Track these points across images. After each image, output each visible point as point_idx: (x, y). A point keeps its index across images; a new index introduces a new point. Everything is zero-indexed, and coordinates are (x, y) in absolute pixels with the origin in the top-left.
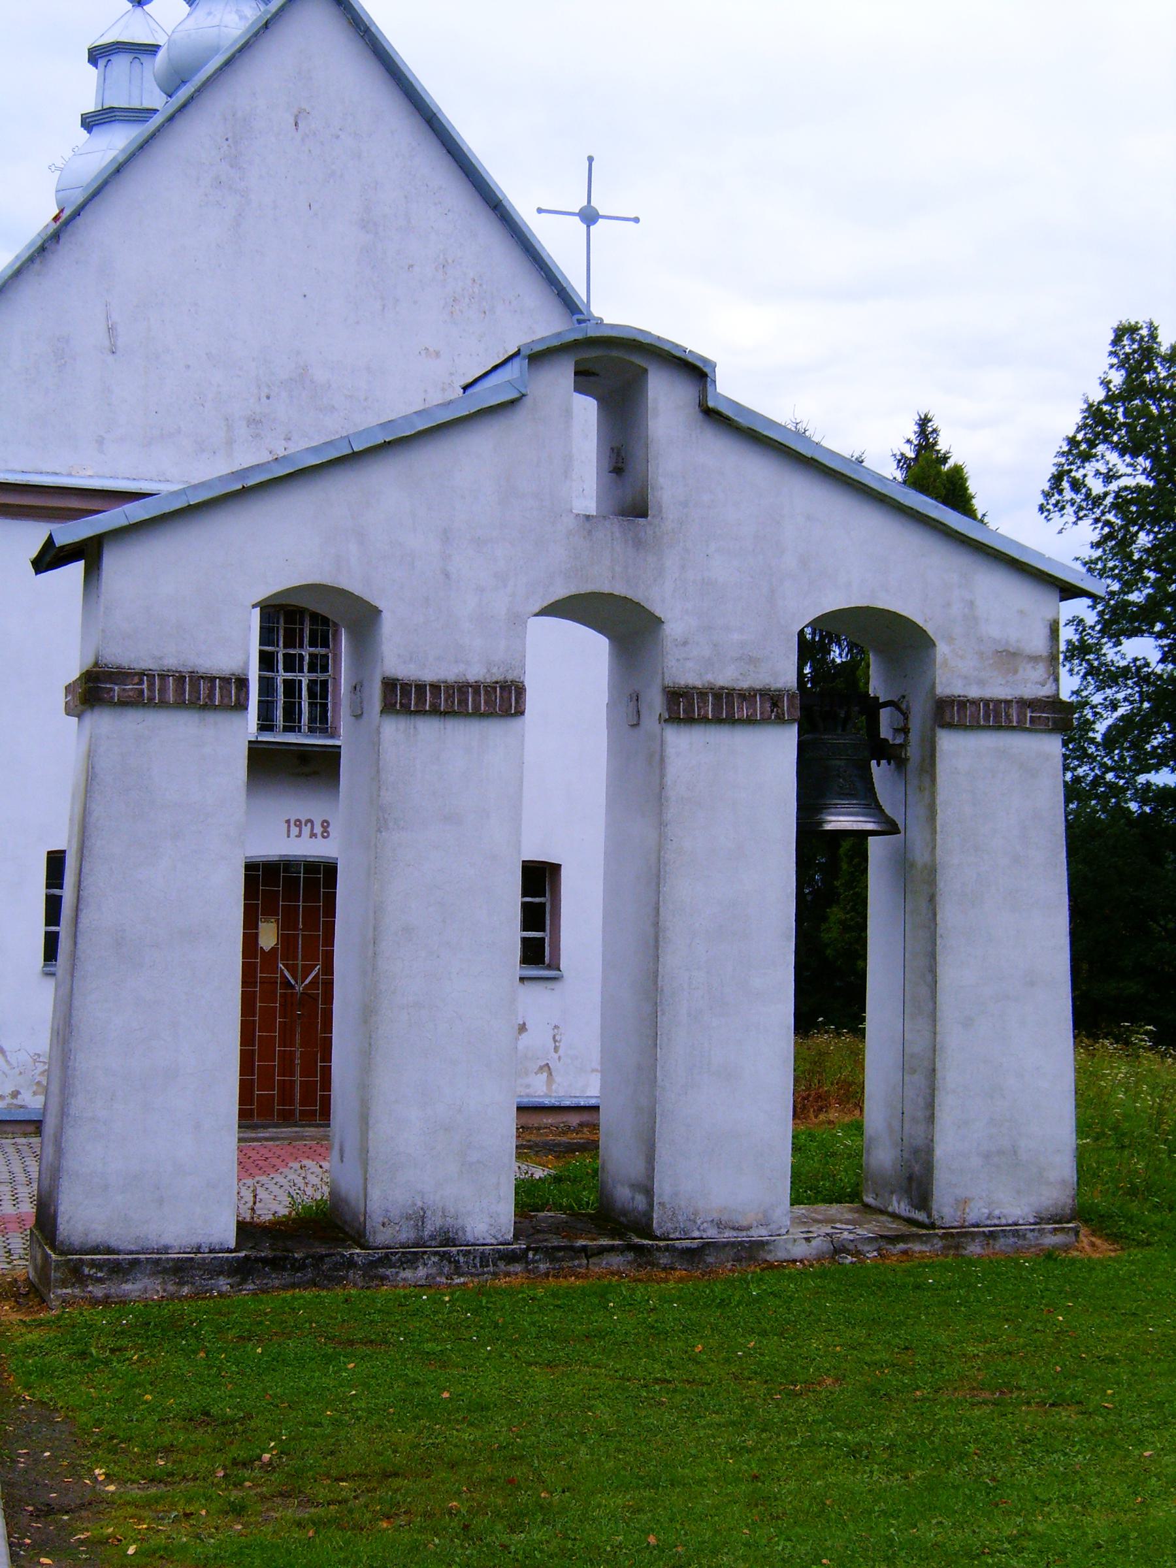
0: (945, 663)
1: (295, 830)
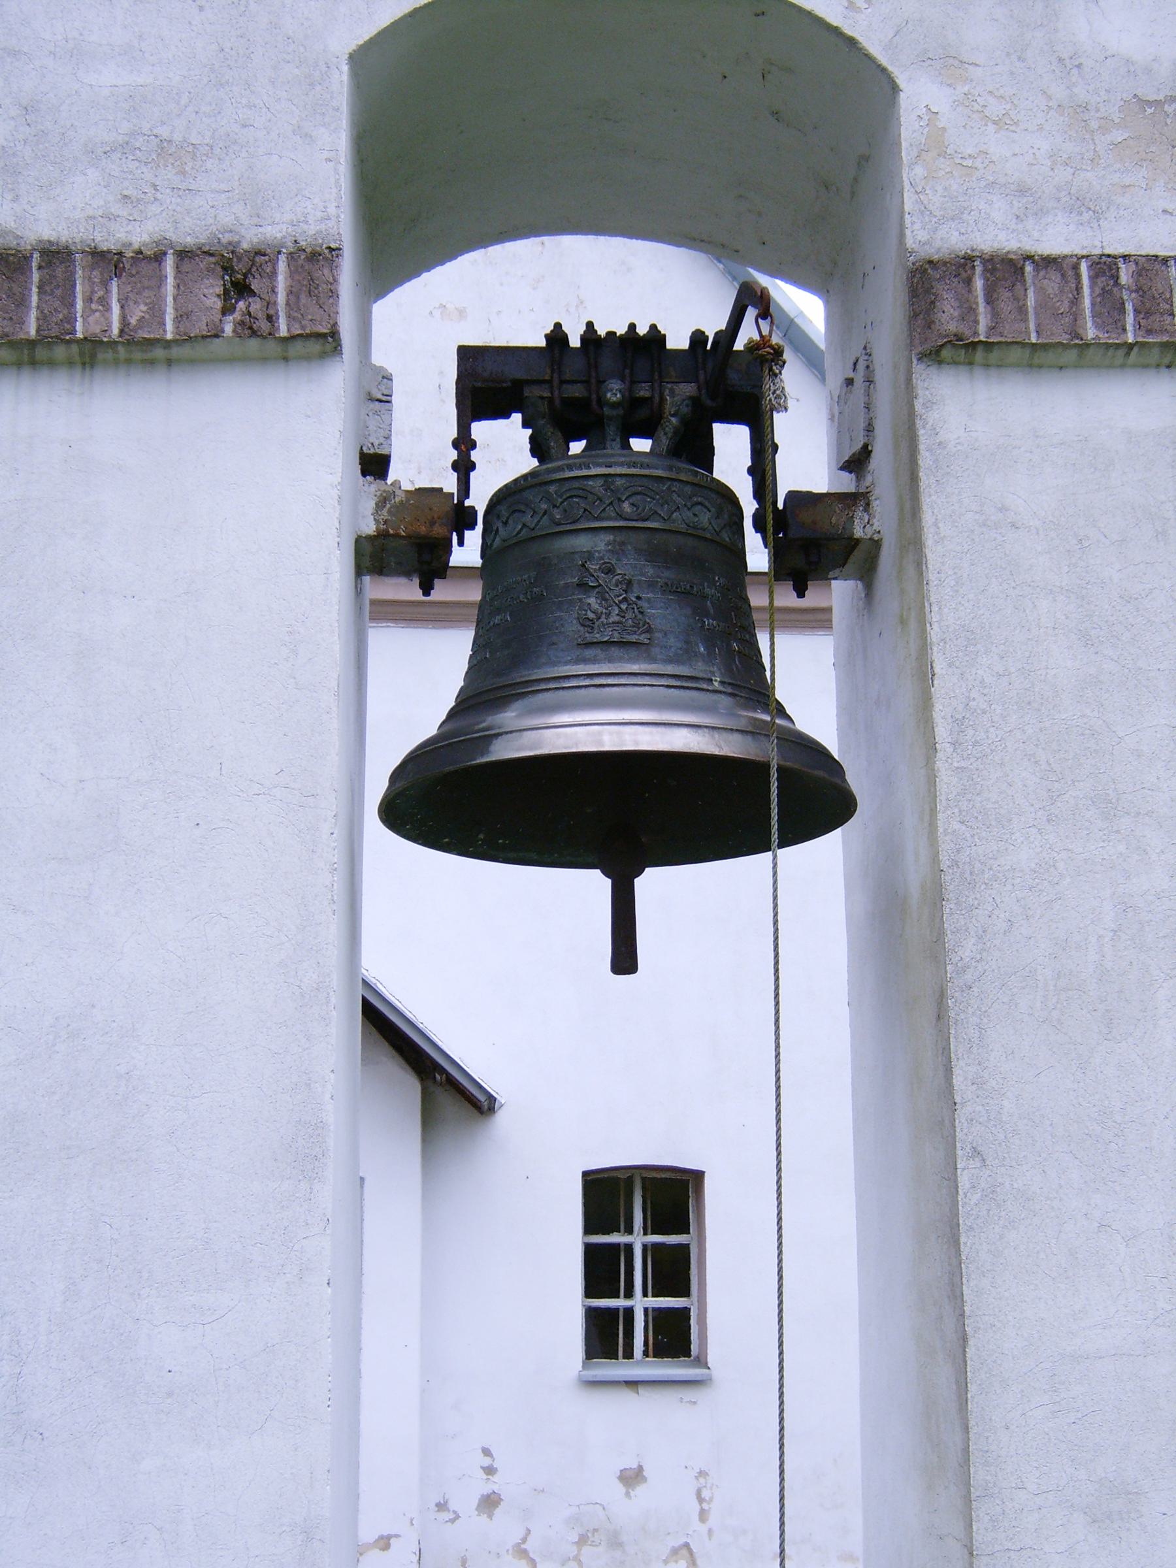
0: (936, 143)
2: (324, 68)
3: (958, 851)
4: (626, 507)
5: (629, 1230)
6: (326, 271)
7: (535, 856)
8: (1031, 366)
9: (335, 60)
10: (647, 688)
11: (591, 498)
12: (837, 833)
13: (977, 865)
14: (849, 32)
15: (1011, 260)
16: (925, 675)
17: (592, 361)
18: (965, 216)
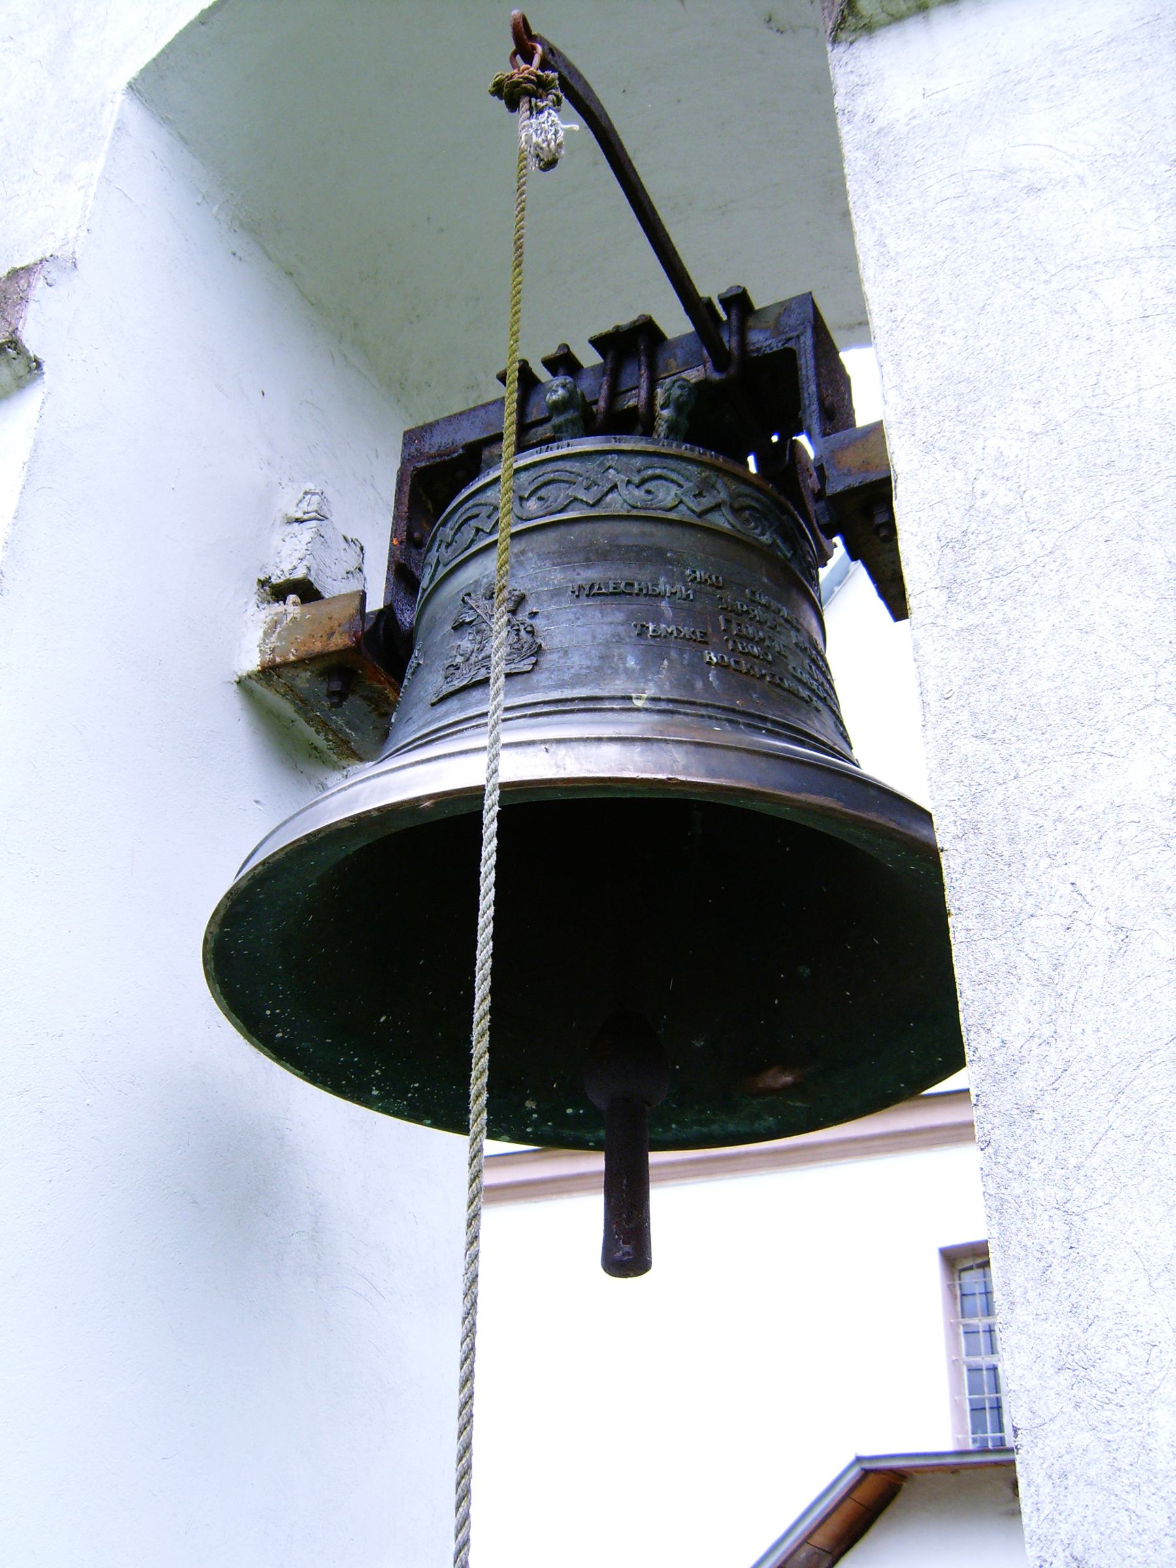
3: (975, 799)
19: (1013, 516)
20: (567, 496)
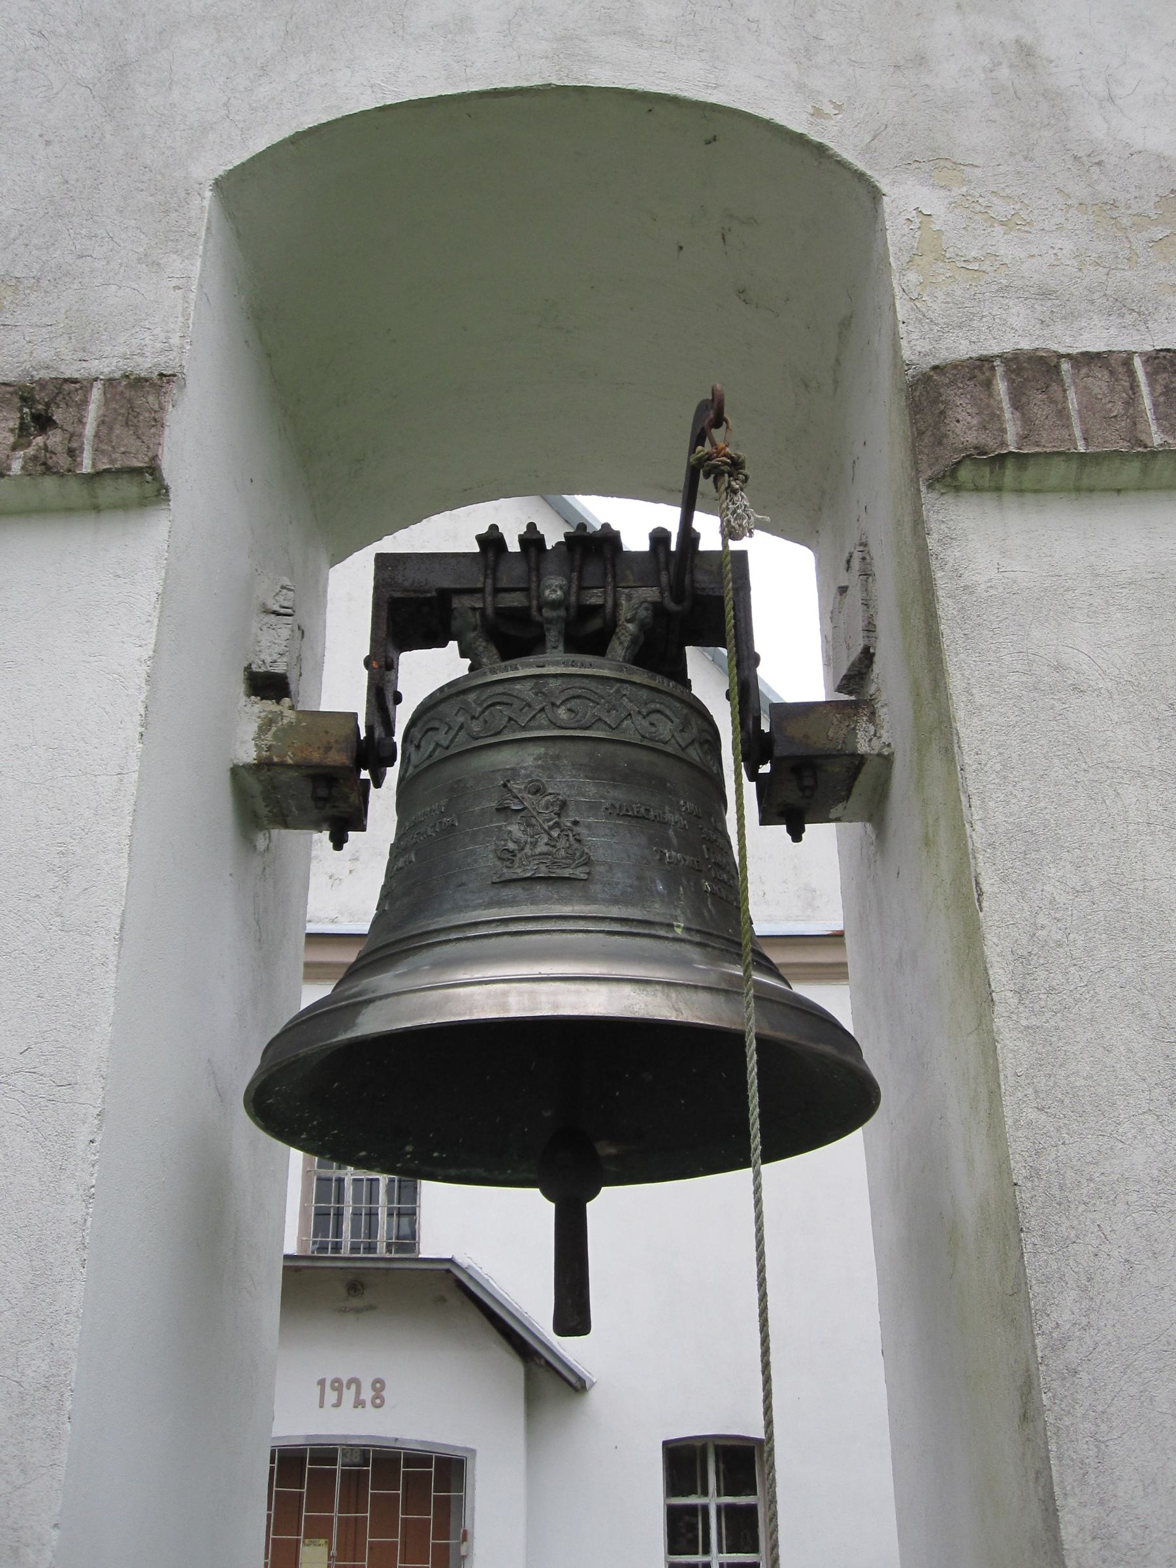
1: (331, 1396)
2: (183, 195)
4: (562, 713)
5: (705, 1493)
6: (151, 398)
7: (481, 1172)
8: (1078, 490)
9: (196, 186)
10: (580, 935)
11: (517, 704)
12: (857, 1136)
13: (1070, 1174)
14: (815, 137)
15: (1041, 358)
16: (966, 897)
17: (533, 565)
18: (975, 323)
19: (1061, 950)
20: (594, 715)
